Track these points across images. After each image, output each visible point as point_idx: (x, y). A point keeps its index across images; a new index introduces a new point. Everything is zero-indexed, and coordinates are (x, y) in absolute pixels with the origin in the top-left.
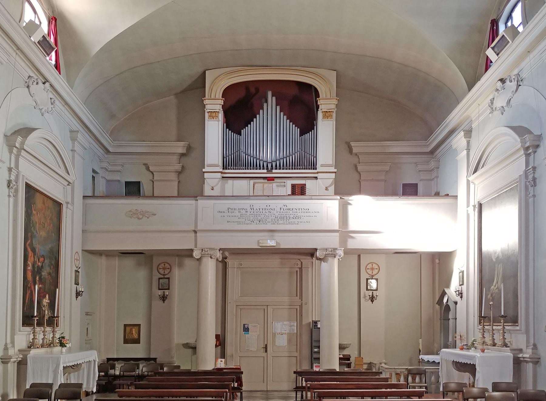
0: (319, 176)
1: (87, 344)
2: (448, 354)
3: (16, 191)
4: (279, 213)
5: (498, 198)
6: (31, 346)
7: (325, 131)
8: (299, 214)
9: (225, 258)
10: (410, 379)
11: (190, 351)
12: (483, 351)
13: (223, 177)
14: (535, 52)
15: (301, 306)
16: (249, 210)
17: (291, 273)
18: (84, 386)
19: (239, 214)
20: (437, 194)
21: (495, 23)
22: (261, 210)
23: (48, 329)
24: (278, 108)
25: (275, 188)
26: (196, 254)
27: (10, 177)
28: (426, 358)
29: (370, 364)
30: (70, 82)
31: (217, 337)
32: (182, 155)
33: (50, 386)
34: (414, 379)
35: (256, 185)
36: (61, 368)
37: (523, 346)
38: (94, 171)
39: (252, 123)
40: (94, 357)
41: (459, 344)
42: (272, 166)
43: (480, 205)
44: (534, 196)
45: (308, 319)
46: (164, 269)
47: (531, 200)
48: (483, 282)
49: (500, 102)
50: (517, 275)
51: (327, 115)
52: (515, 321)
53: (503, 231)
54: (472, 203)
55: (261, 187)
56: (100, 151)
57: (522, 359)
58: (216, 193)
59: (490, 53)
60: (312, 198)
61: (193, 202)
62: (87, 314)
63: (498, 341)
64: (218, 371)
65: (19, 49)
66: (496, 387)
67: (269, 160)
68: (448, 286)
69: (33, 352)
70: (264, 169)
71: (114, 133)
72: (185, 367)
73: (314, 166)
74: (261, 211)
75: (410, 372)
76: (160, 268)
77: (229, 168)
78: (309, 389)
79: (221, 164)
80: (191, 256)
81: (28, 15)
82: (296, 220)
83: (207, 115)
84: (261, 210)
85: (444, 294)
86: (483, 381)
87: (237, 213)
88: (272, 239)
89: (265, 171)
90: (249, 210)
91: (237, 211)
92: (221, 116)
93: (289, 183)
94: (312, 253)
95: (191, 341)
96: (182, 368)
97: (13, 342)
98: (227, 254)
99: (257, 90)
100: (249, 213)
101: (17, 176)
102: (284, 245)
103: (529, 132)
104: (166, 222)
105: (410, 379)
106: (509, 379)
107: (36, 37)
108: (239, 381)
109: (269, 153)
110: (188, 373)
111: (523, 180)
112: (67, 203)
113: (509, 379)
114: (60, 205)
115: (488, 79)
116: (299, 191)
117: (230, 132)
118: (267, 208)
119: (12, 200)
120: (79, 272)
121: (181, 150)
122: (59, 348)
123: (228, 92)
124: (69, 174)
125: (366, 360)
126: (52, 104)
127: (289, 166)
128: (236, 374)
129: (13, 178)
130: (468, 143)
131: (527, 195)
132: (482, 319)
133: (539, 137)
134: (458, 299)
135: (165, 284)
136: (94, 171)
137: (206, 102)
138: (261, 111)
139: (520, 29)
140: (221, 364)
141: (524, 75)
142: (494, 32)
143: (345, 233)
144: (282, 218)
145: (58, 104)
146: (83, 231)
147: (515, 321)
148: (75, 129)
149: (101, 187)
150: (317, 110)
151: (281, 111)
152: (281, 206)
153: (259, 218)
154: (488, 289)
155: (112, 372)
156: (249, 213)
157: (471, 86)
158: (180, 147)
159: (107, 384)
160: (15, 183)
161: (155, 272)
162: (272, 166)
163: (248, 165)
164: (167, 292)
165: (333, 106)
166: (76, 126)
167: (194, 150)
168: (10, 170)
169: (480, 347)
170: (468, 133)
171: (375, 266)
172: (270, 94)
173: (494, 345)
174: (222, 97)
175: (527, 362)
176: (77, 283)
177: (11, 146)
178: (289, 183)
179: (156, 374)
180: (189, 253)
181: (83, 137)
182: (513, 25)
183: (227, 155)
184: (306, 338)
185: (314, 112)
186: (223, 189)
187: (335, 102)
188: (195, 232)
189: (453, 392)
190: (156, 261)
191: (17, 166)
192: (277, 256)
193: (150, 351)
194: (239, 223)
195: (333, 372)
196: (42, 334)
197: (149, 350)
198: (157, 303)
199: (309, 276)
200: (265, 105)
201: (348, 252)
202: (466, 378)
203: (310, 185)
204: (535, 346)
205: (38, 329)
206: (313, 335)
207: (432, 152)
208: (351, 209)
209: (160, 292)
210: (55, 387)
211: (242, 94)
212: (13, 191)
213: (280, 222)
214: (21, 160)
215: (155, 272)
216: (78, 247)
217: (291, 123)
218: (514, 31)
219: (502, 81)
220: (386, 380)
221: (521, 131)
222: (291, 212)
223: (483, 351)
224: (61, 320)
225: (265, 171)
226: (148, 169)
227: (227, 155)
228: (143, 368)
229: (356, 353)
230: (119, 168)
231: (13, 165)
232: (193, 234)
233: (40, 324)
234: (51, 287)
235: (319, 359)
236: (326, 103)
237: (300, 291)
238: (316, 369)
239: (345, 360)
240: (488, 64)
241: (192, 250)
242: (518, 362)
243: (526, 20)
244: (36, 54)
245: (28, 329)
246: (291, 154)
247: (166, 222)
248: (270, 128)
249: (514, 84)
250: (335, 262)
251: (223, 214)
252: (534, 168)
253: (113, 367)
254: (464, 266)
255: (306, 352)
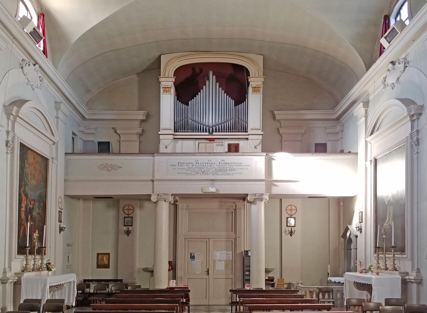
0: (250, 137)
1: (68, 269)
2: (350, 277)
3: (13, 149)
4: (218, 166)
5: (389, 154)
6: (24, 270)
7: (254, 102)
8: (234, 167)
9: (176, 201)
10: (321, 296)
11: (149, 274)
12: (378, 274)
13: (174, 138)
14: (418, 41)
15: (235, 239)
16: (195, 164)
17: (227, 213)
18: (66, 301)
19: (187, 167)
20: (342, 152)
21: (387, 18)
22: (204, 164)
23: (38, 257)
24: (218, 84)
25: (215, 147)
26: (154, 198)
27: (8, 138)
28: (333, 279)
29: (289, 284)
30: (55, 64)
31: (170, 263)
32: (143, 121)
33: (39, 301)
34: (324, 296)
35: (200, 144)
36: (48, 287)
37: (409, 270)
38: (73, 134)
39: (197, 96)
40: (73, 279)
41: (359, 268)
42: (213, 129)
43: (376, 160)
44: (418, 153)
45: (241, 249)
46: (128, 210)
47: (415, 156)
48: (378, 220)
49: (391, 80)
50: (404, 215)
51: (256, 90)
52: (402, 250)
53: (393, 180)
54: (369, 158)
55: (204, 146)
56: (78, 118)
57: (408, 280)
58: (169, 150)
59: (383, 41)
60: (244, 154)
61: (151, 158)
62: (68, 245)
63: (390, 267)
64: (171, 290)
65: (14, 38)
66: (388, 302)
67: (211, 125)
68: (350, 223)
69: (26, 275)
70: (206, 132)
71: (89, 104)
72: (144, 286)
73: (245, 129)
74: (204, 164)
75: (320, 290)
76: (125, 209)
77: (179, 131)
78: (242, 303)
79: (173, 128)
80: (149, 200)
81: (22, 12)
82: (232, 172)
83: (162, 90)
84: (204, 164)
85: (347, 229)
86: (378, 297)
87: (185, 166)
88: (213, 186)
89: (207, 133)
90: (195, 164)
91: (185, 165)
92: (173, 90)
93: (226, 143)
94: (244, 197)
95: (150, 266)
96: (142, 287)
97: (10, 267)
98: (177, 198)
99: (201, 70)
100: (194, 166)
101: (13, 138)
102: (222, 191)
103: (414, 103)
104: (130, 173)
105: (321, 296)
106: (398, 296)
107: (28, 29)
108: (187, 297)
109: (210, 120)
110: (147, 291)
111: (409, 140)
112: (53, 158)
113: (398, 296)
114: (47, 160)
115: (382, 62)
116: (234, 149)
117: (180, 103)
118: (209, 162)
119: (9, 156)
120: (62, 212)
121: (142, 117)
122: (46, 272)
123: (178, 72)
124: (54, 136)
125: (287, 281)
126: (41, 81)
127: (226, 129)
128: (185, 292)
129: (10, 139)
130: (366, 112)
131: (412, 152)
132: (377, 249)
133: (422, 107)
134: (358, 233)
135: (129, 222)
136: (73, 134)
137: (161, 80)
138: (204, 87)
139: (407, 23)
140: (173, 284)
141: (409, 59)
142: (387, 25)
143: (270, 182)
144: (221, 170)
145: (46, 81)
146: (65, 181)
147: (402, 250)
148: (59, 100)
149: (79, 146)
150: (248, 86)
151: (219, 87)
152: (220, 161)
153: (203, 170)
154: (382, 226)
155: (87, 290)
156: (194, 166)
157: (368, 67)
158: (141, 115)
159: (84, 300)
160: (11, 143)
161: (121, 212)
162: (213, 129)
163: (194, 129)
164: (130, 228)
165: (261, 83)
166: (60, 98)
167: (152, 117)
168: (8, 132)
169: (375, 271)
170: (366, 104)
171: (293, 208)
172: (211, 73)
173: (387, 269)
174: (174, 76)
175: (412, 282)
176: (60, 221)
177: (8, 114)
178: (226, 143)
179: (122, 292)
180: (148, 198)
181: (65, 107)
182: (401, 20)
183: (178, 121)
184: (239, 264)
185: (246, 87)
186: (174, 147)
187: (262, 79)
188: (153, 181)
189: (355, 306)
190: (122, 204)
191: (13, 130)
192: (216, 200)
194: (187, 174)
195: (260, 291)
196: (33, 260)
197: (117, 273)
198: (123, 237)
199: (242, 215)
200: (207, 82)
201: (272, 197)
202: (364, 295)
203: (242, 144)
204: (418, 270)
205: (30, 257)
206: (245, 261)
207: (338, 119)
208: (274, 163)
209: (125, 228)
210: (43, 302)
211: (189, 73)
212: (10, 149)
213: (219, 173)
214: (16, 125)
215: (121, 212)
216: (61, 193)
217: (228, 96)
218: (402, 24)
219: (393, 63)
220: (302, 296)
221: (407, 102)
222: (228, 166)
223: (378, 274)
224: (48, 250)
225: (207, 133)
226: (116, 132)
227: (178, 121)
228: (112, 288)
229: (279, 275)
230: (93, 131)
231: (10, 129)
232: (151, 183)
233: (31, 253)
234: (40, 224)
235: (249, 280)
236: (255, 81)
237: (234, 227)
238: (247, 288)
239: (270, 281)
240: (382, 50)
241: (150, 195)
242: (405, 283)
243: (411, 16)
244: (28, 42)
245: (22, 257)
246: (228, 120)
247: (130, 173)
248: (211, 100)
249: (402, 65)
250: (262, 205)
251: (174, 167)
252: (418, 131)
253: (89, 287)
254: (363, 207)
255: (239, 274)
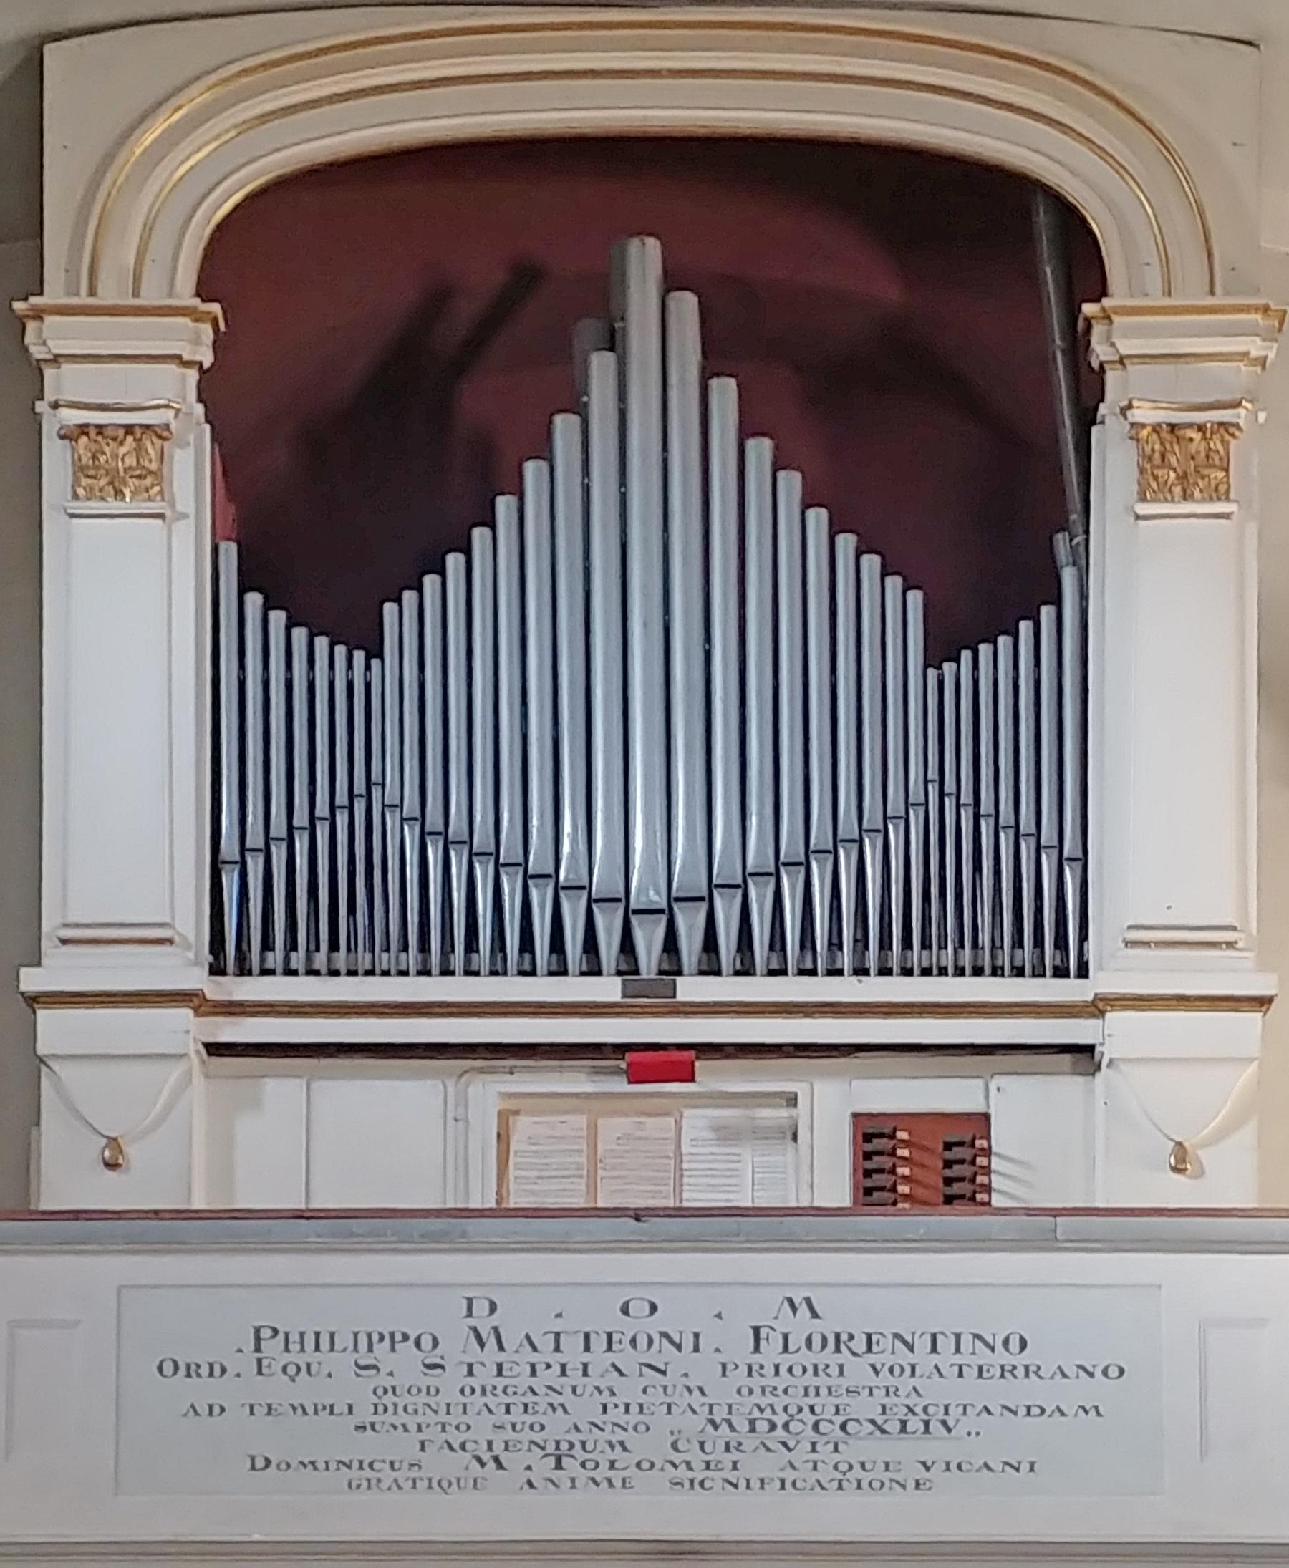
0: (1116, 1034)
4: (738, 1377)
8: (937, 1392)
13: (214, 1049)
16: (456, 1347)
19: (361, 1391)
22: (572, 1345)
24: (725, 391)
25: (700, 1146)
35: (523, 1126)
39: (480, 536)
42: (671, 944)
55: (571, 1138)
60: (1051, 1226)
70: (595, 971)
73: (1061, 942)
74: (573, 1352)
77: (275, 959)
79: (191, 922)
82: (906, 1452)
83: (56, 460)
84: (572, 1345)
87: (339, 1380)
89: (608, 988)
90: (456, 1347)
91: (342, 1363)
92: (190, 468)
93: (829, 1105)
100: (452, 1379)
109: (644, 830)
116: (923, 1171)
117: (278, 618)
118: (627, 1327)
123: (258, 249)
127: (835, 944)
137: (50, 337)
138: (564, 427)
140: (585, 1154)
144: (772, 1427)
150: (1087, 419)
151: (746, 431)
152: (766, 1309)
153: (557, 1427)
156: (452, 1379)
162: (671, 944)
163: (446, 940)
172: (644, 260)
174: (204, 291)
178: (829, 1105)
183: (255, 838)
185: (1058, 470)
193: (1152, 1059)
194: (362, 1474)
200: (601, 365)
203: (1030, 1126)
213: (757, 1464)
217: (847, 543)
222: (859, 1372)
225: (608, 988)
227: (255, 838)
246: (848, 826)
248: (656, 561)
251: (204, 1390)
